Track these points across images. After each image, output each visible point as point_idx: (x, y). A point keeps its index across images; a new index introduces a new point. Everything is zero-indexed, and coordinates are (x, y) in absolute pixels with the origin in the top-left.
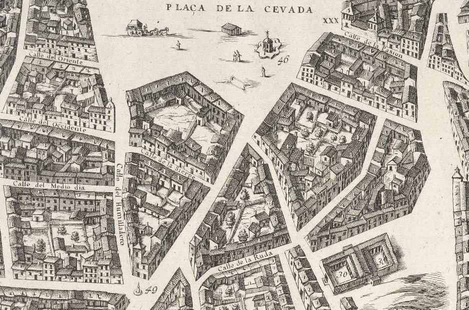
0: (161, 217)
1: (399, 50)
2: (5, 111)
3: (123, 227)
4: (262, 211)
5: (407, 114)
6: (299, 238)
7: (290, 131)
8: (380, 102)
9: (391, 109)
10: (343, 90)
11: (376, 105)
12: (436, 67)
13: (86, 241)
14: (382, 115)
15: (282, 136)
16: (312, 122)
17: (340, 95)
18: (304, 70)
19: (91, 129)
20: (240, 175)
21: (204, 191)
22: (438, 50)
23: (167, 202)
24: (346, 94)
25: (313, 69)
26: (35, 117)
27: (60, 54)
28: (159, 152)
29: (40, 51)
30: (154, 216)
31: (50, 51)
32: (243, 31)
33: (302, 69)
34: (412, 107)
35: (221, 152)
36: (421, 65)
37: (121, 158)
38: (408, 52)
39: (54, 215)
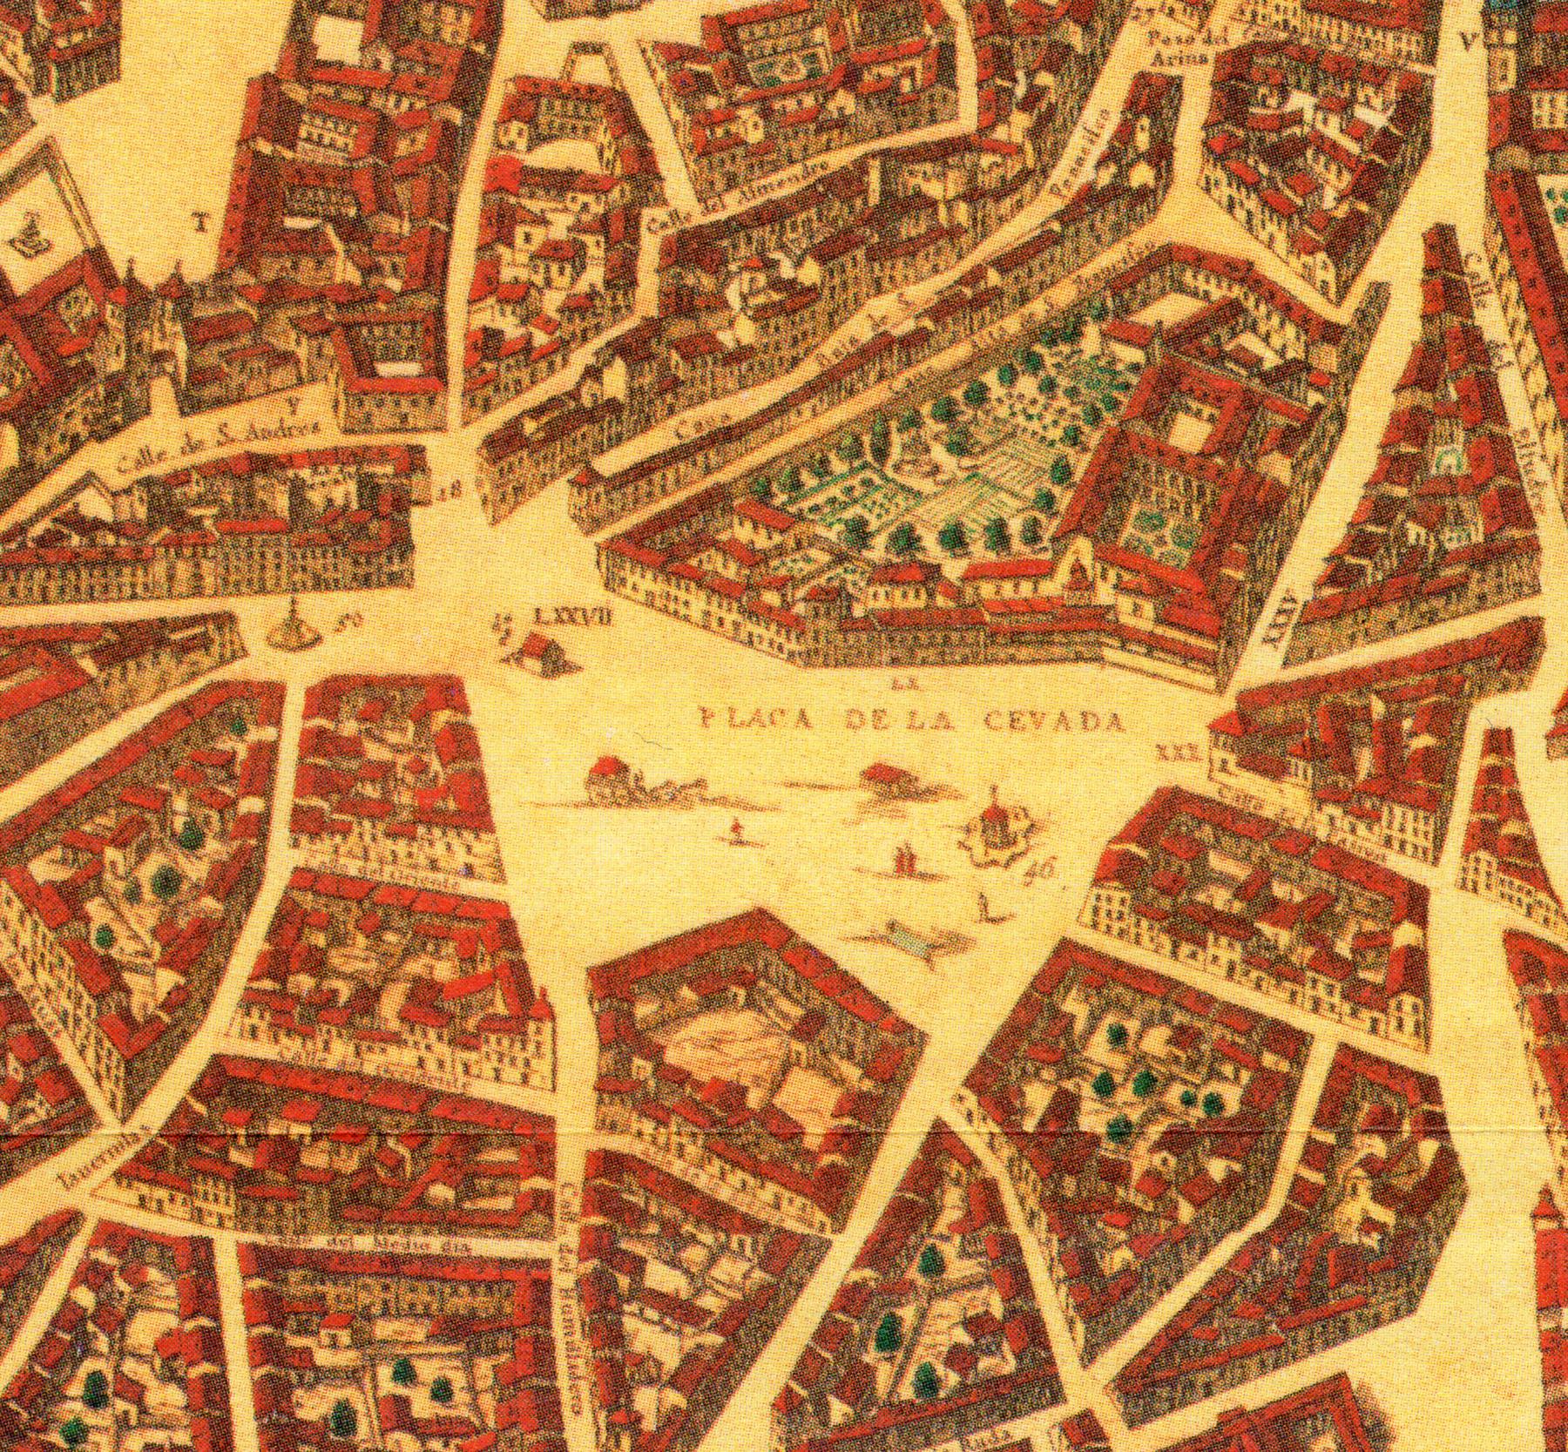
0: (689, 1330)
1: (1374, 839)
2: (235, 1031)
3: (580, 1362)
4: (981, 1310)
5: (1400, 1026)
6: (1087, 1386)
7: (1060, 1077)
8: (1321, 992)
9: (1354, 1014)
10: (1215, 958)
11: (1308, 1005)
12: (1482, 887)
13: (475, 1406)
14: (1329, 1031)
15: (1038, 1097)
16: (1126, 1052)
17: (1210, 971)
18: (1098, 898)
19: (492, 1081)
20: (911, 1212)
21: (811, 1252)
22: (1482, 837)
23: (706, 1287)
24: (1223, 972)
25: (1127, 895)
26: (327, 1048)
27: (395, 861)
28: (681, 1147)
29: (336, 851)
30: (667, 1329)
31: (366, 850)
32: (922, 785)
33: (1093, 901)
34: (1415, 1008)
35: (858, 1138)
36: (1440, 880)
37: (570, 1165)
38: (1403, 844)
39: (384, 1329)
